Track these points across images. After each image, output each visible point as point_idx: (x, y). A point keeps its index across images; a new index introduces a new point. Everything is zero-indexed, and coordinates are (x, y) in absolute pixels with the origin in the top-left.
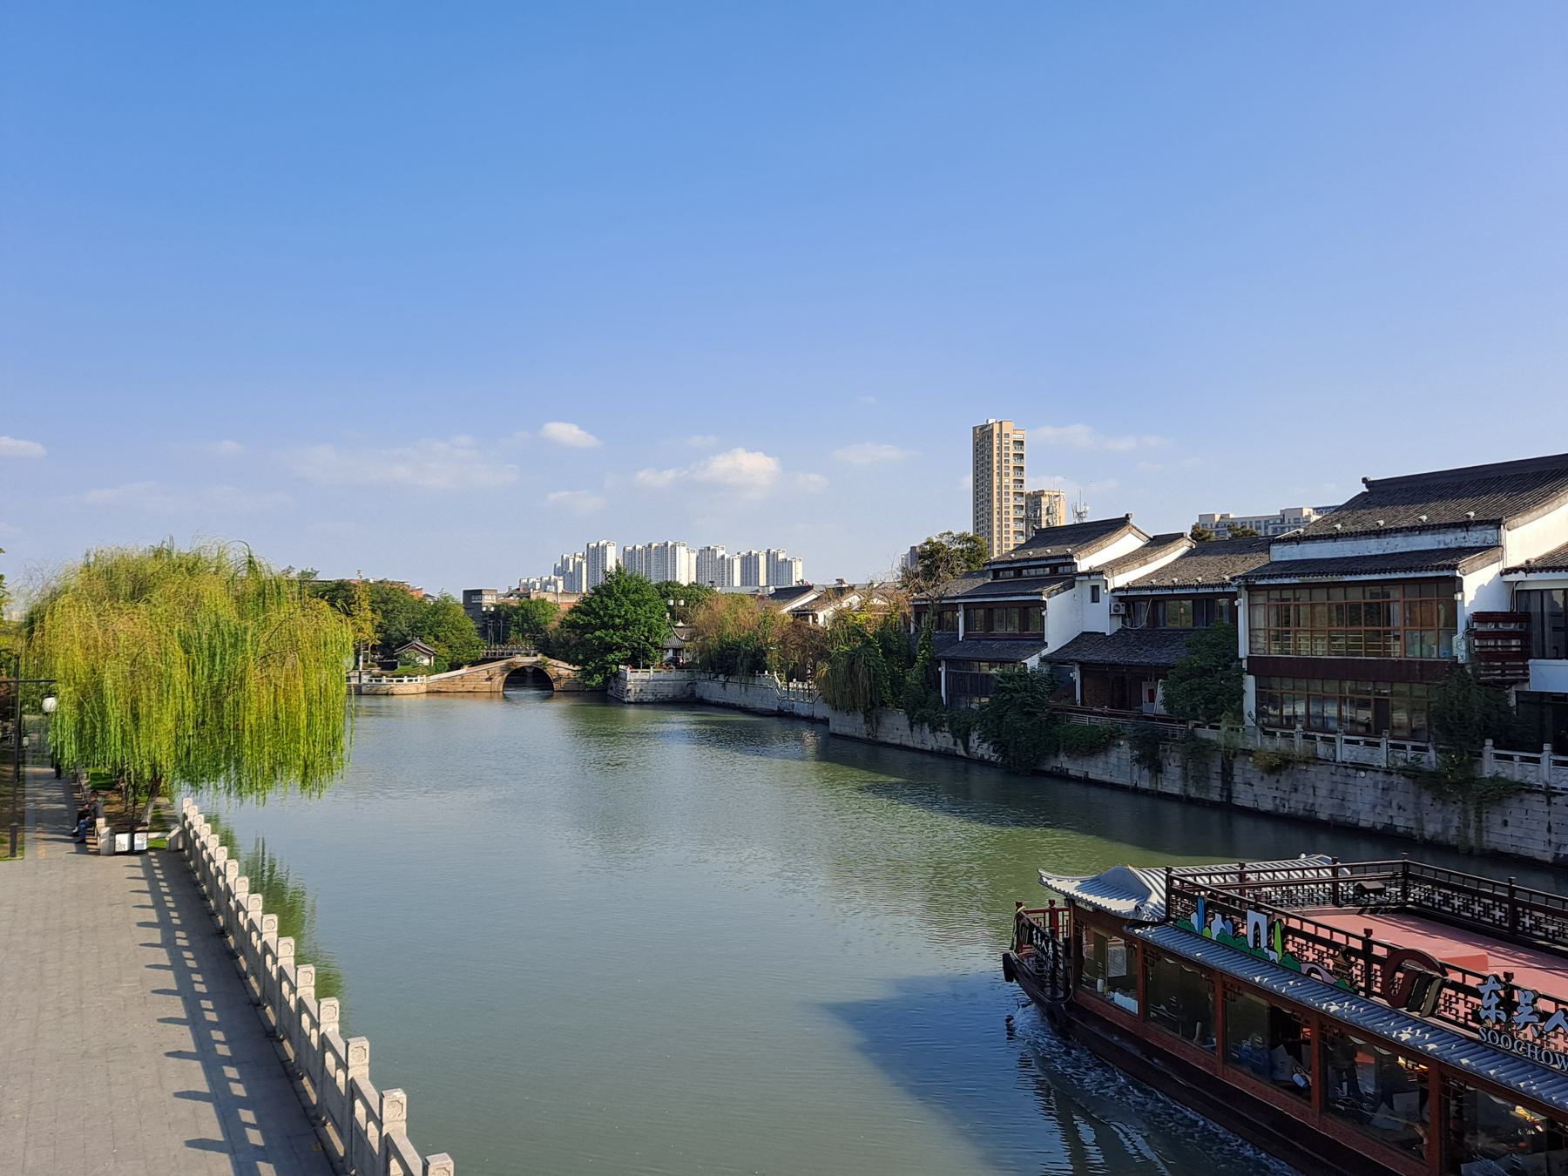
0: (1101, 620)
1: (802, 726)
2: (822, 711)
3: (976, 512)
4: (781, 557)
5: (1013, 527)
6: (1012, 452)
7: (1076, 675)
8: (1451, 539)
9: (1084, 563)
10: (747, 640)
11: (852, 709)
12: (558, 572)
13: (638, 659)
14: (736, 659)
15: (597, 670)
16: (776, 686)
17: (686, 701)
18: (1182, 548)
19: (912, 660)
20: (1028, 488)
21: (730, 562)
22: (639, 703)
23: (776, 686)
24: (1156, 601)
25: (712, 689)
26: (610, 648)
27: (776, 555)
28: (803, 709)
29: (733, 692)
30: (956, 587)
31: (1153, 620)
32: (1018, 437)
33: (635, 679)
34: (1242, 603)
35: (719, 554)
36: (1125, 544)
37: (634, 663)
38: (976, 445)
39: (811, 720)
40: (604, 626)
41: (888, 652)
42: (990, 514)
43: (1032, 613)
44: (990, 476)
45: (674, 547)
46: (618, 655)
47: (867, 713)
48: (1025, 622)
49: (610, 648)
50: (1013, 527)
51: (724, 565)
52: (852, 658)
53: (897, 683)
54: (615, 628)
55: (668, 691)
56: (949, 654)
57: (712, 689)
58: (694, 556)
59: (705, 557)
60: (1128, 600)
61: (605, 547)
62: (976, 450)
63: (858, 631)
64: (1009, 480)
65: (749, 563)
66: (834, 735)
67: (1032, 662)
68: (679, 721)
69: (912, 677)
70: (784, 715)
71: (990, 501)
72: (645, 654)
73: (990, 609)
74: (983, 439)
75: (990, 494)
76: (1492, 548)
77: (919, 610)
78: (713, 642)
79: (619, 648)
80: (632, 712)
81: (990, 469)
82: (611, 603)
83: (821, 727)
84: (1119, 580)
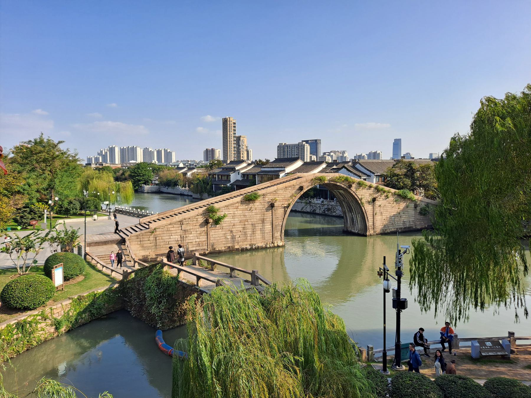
0: (239, 178)
1: (186, 197)
2: (190, 194)
3: (223, 141)
4: (168, 151)
5: (233, 146)
6: (233, 125)
7: (235, 187)
8: (281, 169)
9: (237, 168)
10: (173, 179)
11: (197, 193)
12: (99, 154)
13: (146, 183)
14: (172, 183)
15: (137, 186)
16: (180, 189)
17: (158, 192)
18: (253, 166)
19: (208, 184)
20: (237, 135)
21: (153, 152)
22: (148, 193)
23: (180, 189)
24: (248, 175)
25: (164, 189)
26: (140, 181)
27: (167, 150)
28: (186, 193)
29: (170, 190)
30: (216, 171)
31: (247, 178)
32: (234, 122)
33: (147, 187)
34: (257, 177)
35: (150, 149)
36: (244, 165)
37: (145, 183)
38: (223, 123)
39: (188, 195)
40: (138, 176)
41: (204, 183)
42: (227, 142)
43: (228, 176)
44: (227, 132)
45: (136, 148)
46: (142, 182)
47: (200, 193)
48: (227, 178)
49: (140, 181)
50: (233, 146)
51: (151, 153)
52: (197, 184)
53: (205, 188)
54: (141, 176)
55: (154, 190)
56: (215, 183)
57: (164, 189)
58: (142, 150)
59: (147, 153)
60: (244, 175)
61: (114, 148)
62: (223, 125)
63: (198, 179)
64: (232, 133)
65: (159, 152)
66: (194, 198)
67: (228, 185)
68: (157, 197)
69: (208, 187)
70: (182, 195)
71: (227, 138)
72: (148, 182)
73: (222, 176)
74: (225, 122)
75: (227, 137)
76: (284, 171)
77: (209, 175)
78: (165, 180)
79: (142, 180)
80: (146, 195)
81: (227, 130)
82: (139, 171)
83: (189, 197)
84: (242, 171)
